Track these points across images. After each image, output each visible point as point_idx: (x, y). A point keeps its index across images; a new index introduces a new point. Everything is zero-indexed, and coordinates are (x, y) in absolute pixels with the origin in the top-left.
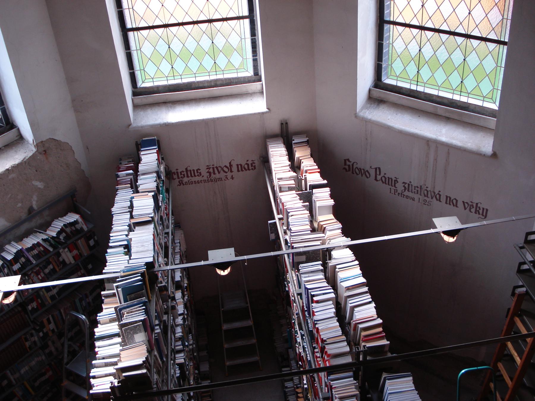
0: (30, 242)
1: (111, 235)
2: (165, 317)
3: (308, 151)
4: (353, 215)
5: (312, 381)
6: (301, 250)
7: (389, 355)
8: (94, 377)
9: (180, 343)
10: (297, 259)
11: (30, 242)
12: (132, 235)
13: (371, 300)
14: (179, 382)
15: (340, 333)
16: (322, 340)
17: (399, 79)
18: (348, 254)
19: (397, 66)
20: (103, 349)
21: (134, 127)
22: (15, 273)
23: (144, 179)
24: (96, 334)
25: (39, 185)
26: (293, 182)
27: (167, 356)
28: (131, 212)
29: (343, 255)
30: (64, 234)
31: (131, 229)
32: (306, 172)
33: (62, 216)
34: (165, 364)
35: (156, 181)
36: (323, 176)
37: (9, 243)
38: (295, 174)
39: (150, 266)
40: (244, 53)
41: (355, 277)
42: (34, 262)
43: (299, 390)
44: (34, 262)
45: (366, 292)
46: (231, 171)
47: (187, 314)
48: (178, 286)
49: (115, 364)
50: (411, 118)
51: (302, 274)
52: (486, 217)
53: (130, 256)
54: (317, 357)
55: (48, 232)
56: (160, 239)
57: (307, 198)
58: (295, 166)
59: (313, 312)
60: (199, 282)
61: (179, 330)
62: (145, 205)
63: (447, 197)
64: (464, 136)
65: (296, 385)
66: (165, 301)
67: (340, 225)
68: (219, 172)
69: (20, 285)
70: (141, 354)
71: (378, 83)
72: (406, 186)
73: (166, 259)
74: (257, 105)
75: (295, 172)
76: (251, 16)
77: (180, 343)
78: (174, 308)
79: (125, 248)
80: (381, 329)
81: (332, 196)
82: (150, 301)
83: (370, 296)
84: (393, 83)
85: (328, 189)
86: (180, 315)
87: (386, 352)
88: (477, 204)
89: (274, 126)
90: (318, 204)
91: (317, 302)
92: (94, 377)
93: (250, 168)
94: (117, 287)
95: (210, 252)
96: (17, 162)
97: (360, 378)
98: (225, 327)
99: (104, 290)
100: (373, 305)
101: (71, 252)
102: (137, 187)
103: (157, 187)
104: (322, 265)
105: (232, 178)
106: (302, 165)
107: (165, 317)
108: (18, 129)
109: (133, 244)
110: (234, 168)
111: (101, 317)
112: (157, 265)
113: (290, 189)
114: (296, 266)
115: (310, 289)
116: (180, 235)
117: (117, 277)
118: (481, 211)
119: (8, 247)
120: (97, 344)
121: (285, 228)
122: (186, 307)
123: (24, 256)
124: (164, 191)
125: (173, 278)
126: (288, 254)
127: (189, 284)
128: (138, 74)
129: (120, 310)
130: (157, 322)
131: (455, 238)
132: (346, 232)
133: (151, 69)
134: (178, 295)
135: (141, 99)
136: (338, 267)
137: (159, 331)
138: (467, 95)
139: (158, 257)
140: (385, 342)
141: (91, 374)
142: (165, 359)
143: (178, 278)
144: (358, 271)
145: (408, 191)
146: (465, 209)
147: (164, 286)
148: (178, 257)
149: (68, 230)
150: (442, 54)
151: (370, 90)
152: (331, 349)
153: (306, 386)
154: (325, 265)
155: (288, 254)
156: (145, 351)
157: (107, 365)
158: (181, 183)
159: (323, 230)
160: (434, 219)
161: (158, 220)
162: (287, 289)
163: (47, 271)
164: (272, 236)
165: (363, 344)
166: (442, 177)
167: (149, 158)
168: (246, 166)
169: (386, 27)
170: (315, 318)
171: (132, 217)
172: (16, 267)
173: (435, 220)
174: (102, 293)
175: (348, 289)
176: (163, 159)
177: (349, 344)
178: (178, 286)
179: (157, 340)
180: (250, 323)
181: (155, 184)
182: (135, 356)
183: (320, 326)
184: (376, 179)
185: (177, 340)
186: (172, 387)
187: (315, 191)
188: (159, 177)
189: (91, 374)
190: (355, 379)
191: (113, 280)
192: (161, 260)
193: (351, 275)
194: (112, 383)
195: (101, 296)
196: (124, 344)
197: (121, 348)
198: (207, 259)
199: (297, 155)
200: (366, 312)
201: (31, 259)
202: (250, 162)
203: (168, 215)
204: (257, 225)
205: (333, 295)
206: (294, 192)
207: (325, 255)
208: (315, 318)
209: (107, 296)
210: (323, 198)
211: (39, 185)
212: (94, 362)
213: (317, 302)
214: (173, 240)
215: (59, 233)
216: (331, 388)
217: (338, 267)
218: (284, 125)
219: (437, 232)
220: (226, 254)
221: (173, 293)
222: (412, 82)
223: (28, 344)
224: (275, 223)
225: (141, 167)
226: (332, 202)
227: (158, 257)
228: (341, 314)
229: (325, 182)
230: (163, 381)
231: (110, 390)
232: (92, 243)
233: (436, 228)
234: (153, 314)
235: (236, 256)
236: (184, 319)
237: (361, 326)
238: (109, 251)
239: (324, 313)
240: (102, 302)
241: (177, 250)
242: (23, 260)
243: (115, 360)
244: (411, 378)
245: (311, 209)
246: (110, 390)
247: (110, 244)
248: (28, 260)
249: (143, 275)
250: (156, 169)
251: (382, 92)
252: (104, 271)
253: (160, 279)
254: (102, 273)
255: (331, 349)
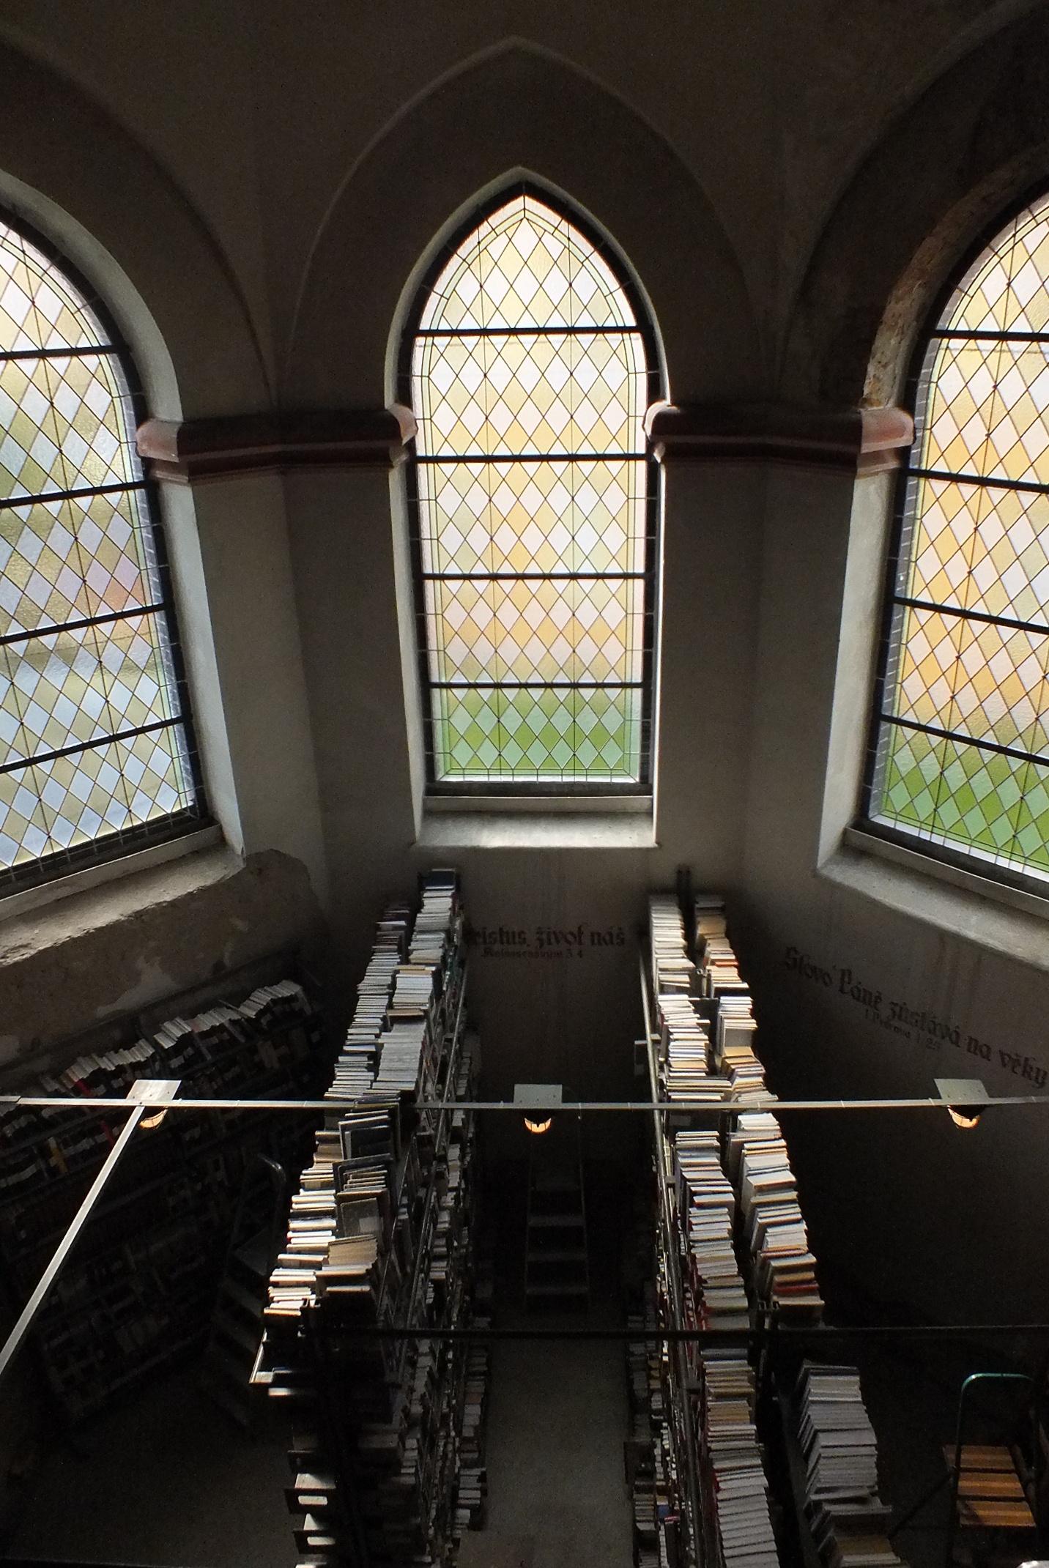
0: (207, 1021)
1: (350, 1031)
2: (422, 1193)
3: (721, 926)
4: (788, 1053)
5: (673, 1350)
6: (683, 1106)
7: (822, 1326)
8: (276, 1285)
9: (443, 1242)
10: (675, 1121)
11: (207, 1021)
12: (385, 1038)
13: (800, 1216)
14: (430, 1317)
15: (735, 1270)
16: (699, 1278)
17: (900, 818)
18: (770, 1121)
19: (899, 796)
20: (304, 1236)
21: (422, 848)
22: (169, 1075)
23: (422, 940)
24: (294, 1206)
25: (241, 925)
26: (686, 978)
27: (414, 1265)
28: (391, 995)
29: (759, 1125)
30: (268, 1017)
31: (387, 1025)
32: (713, 963)
33: (271, 985)
34: (408, 1278)
35: (443, 946)
36: (743, 976)
37: (171, 1018)
38: (691, 965)
39: (408, 1097)
40: (627, 746)
41: (776, 1170)
42: (209, 1057)
43: (654, 1364)
44: (209, 1057)
45: (792, 1202)
46: (580, 943)
47: (465, 1190)
48: (455, 1136)
49: (318, 1266)
50: (913, 889)
51: (681, 1150)
52: (1043, 1084)
53: (376, 1075)
54: (689, 1309)
55: (242, 1009)
56: (434, 1050)
57: (708, 1009)
58: (694, 950)
59: (691, 1223)
60: (494, 1139)
61: (445, 1217)
62: (416, 986)
63: (971, 1038)
64: (1011, 934)
65: (650, 1353)
66: (426, 1162)
67: (762, 1070)
68: (558, 942)
69: (176, 1097)
70: (367, 1257)
71: (861, 819)
72: (897, 1009)
73: (440, 1086)
74: (639, 837)
75: (692, 959)
76: (647, 684)
77: (443, 1242)
78: (441, 1176)
79: (369, 1059)
80: (811, 1275)
81: (754, 1014)
82: (398, 1160)
83: (798, 1210)
84: (889, 823)
85: (748, 999)
86: (452, 1190)
87: (817, 1321)
88: (1027, 1059)
89: (665, 872)
90: (728, 1024)
91: (701, 1206)
92: (276, 1285)
93: (615, 941)
94: (344, 1128)
95: (517, 1087)
96: (209, 882)
97: (762, 1361)
98: (533, 1221)
99: (321, 1129)
100: (804, 1226)
101: (276, 1048)
102: (409, 953)
103: (444, 958)
104: (718, 1139)
105: (580, 954)
106: (708, 949)
107: (422, 1193)
108: (221, 828)
109: (388, 1049)
110: (586, 939)
111: (307, 1175)
112: (420, 1098)
113: (680, 990)
114: (671, 1132)
115: (690, 1180)
116: (473, 1045)
117: (348, 1110)
118: (1033, 1074)
119: (167, 1025)
120: (294, 1224)
121: (662, 1059)
122: (464, 1175)
123: (193, 1046)
124: (455, 964)
125: (448, 1120)
126: (661, 1112)
127: (476, 1134)
128: (440, 759)
129: (343, 1170)
130: (405, 1201)
131: (975, 1121)
132: (771, 1083)
133: (462, 754)
134: (454, 1152)
135: (441, 801)
136: (746, 1146)
137: (406, 1217)
138: (1022, 860)
139: (425, 1083)
140: (816, 1301)
141: (272, 1279)
142: (409, 1269)
143: (458, 1120)
144: (783, 1159)
145: (900, 1017)
146: (1004, 1065)
147: (430, 1136)
148: (463, 1083)
149: (277, 1009)
150: (982, 784)
151: (845, 832)
152: (714, 1299)
153: (666, 1358)
154: (723, 1139)
155: (661, 1112)
156: (374, 1252)
157: (303, 1265)
158: (488, 952)
159: (730, 1075)
160: (937, 1081)
161: (435, 1020)
162: (654, 1169)
163: (228, 1076)
164: (638, 1069)
165: (775, 1298)
166: (965, 1004)
167: (438, 904)
168: (607, 938)
169: (884, 726)
170: (692, 1235)
171: (390, 1006)
172: (175, 1063)
173: (940, 1083)
174: (318, 1133)
175: (762, 1190)
176: (461, 908)
177: (749, 1295)
178: (455, 1136)
179: (399, 1234)
180: (577, 1220)
181: (440, 953)
182: (351, 1261)
183: (699, 1252)
184: (842, 990)
185: (438, 1235)
186: (413, 1322)
187: (723, 999)
188: (449, 939)
189: (272, 1279)
190: (750, 1364)
191: (340, 1113)
192: (429, 1087)
193: (770, 1164)
194: (305, 1300)
195: (314, 1138)
196: (337, 1232)
197: (333, 1239)
198: (510, 1099)
199: (701, 930)
200: (788, 1238)
201: (204, 1050)
202: (615, 931)
203: (456, 1006)
204: (612, 1045)
205: (731, 1198)
206: (685, 997)
207: (724, 1121)
208: (692, 1235)
209: (325, 1140)
210: (738, 1013)
211: (241, 925)
212: (281, 1256)
213: (701, 1206)
214: (459, 1054)
215: (261, 1013)
216: (702, 1373)
217: (746, 1146)
218: (684, 874)
219: (940, 1107)
220: (547, 1096)
221: (444, 1148)
222: (924, 826)
223: (171, 1201)
224: (646, 1046)
225: (421, 919)
226: (752, 1024)
227: (425, 1083)
228: (744, 1234)
229: (745, 986)
230: (398, 1310)
231: (299, 1313)
232: (315, 1037)
233: (940, 1098)
234: (401, 1184)
235: (565, 1100)
236: (457, 1199)
237: (774, 1263)
238: (341, 1059)
239: (711, 1229)
240: (315, 1149)
241: (465, 1070)
242: (190, 1051)
243: (320, 1258)
244: (857, 1378)
245: (712, 1031)
246: (299, 1313)
247: (346, 1048)
248: (198, 1053)
249: (392, 1112)
250: (447, 926)
251: (866, 837)
252: (326, 1095)
253: (424, 1123)
254: (323, 1099)
255: (714, 1299)
